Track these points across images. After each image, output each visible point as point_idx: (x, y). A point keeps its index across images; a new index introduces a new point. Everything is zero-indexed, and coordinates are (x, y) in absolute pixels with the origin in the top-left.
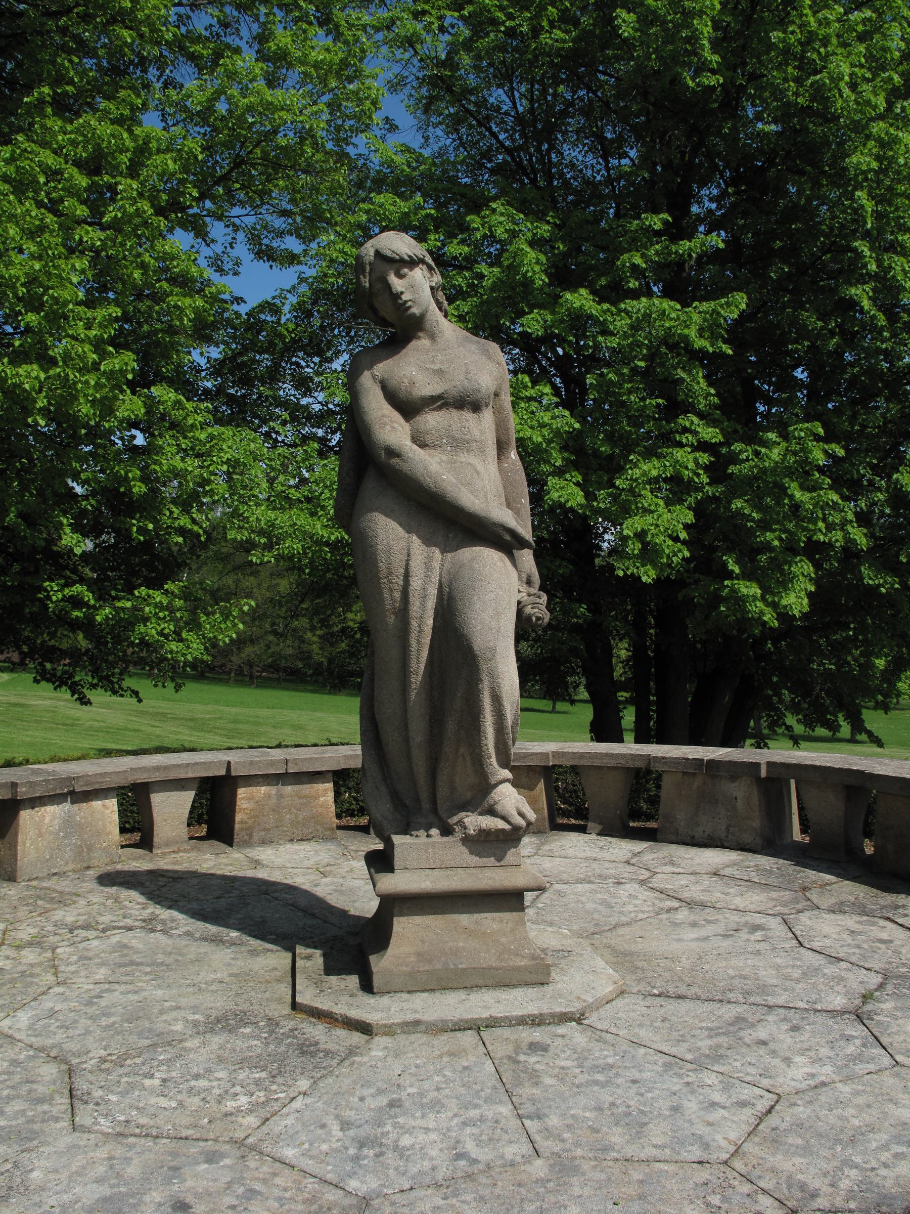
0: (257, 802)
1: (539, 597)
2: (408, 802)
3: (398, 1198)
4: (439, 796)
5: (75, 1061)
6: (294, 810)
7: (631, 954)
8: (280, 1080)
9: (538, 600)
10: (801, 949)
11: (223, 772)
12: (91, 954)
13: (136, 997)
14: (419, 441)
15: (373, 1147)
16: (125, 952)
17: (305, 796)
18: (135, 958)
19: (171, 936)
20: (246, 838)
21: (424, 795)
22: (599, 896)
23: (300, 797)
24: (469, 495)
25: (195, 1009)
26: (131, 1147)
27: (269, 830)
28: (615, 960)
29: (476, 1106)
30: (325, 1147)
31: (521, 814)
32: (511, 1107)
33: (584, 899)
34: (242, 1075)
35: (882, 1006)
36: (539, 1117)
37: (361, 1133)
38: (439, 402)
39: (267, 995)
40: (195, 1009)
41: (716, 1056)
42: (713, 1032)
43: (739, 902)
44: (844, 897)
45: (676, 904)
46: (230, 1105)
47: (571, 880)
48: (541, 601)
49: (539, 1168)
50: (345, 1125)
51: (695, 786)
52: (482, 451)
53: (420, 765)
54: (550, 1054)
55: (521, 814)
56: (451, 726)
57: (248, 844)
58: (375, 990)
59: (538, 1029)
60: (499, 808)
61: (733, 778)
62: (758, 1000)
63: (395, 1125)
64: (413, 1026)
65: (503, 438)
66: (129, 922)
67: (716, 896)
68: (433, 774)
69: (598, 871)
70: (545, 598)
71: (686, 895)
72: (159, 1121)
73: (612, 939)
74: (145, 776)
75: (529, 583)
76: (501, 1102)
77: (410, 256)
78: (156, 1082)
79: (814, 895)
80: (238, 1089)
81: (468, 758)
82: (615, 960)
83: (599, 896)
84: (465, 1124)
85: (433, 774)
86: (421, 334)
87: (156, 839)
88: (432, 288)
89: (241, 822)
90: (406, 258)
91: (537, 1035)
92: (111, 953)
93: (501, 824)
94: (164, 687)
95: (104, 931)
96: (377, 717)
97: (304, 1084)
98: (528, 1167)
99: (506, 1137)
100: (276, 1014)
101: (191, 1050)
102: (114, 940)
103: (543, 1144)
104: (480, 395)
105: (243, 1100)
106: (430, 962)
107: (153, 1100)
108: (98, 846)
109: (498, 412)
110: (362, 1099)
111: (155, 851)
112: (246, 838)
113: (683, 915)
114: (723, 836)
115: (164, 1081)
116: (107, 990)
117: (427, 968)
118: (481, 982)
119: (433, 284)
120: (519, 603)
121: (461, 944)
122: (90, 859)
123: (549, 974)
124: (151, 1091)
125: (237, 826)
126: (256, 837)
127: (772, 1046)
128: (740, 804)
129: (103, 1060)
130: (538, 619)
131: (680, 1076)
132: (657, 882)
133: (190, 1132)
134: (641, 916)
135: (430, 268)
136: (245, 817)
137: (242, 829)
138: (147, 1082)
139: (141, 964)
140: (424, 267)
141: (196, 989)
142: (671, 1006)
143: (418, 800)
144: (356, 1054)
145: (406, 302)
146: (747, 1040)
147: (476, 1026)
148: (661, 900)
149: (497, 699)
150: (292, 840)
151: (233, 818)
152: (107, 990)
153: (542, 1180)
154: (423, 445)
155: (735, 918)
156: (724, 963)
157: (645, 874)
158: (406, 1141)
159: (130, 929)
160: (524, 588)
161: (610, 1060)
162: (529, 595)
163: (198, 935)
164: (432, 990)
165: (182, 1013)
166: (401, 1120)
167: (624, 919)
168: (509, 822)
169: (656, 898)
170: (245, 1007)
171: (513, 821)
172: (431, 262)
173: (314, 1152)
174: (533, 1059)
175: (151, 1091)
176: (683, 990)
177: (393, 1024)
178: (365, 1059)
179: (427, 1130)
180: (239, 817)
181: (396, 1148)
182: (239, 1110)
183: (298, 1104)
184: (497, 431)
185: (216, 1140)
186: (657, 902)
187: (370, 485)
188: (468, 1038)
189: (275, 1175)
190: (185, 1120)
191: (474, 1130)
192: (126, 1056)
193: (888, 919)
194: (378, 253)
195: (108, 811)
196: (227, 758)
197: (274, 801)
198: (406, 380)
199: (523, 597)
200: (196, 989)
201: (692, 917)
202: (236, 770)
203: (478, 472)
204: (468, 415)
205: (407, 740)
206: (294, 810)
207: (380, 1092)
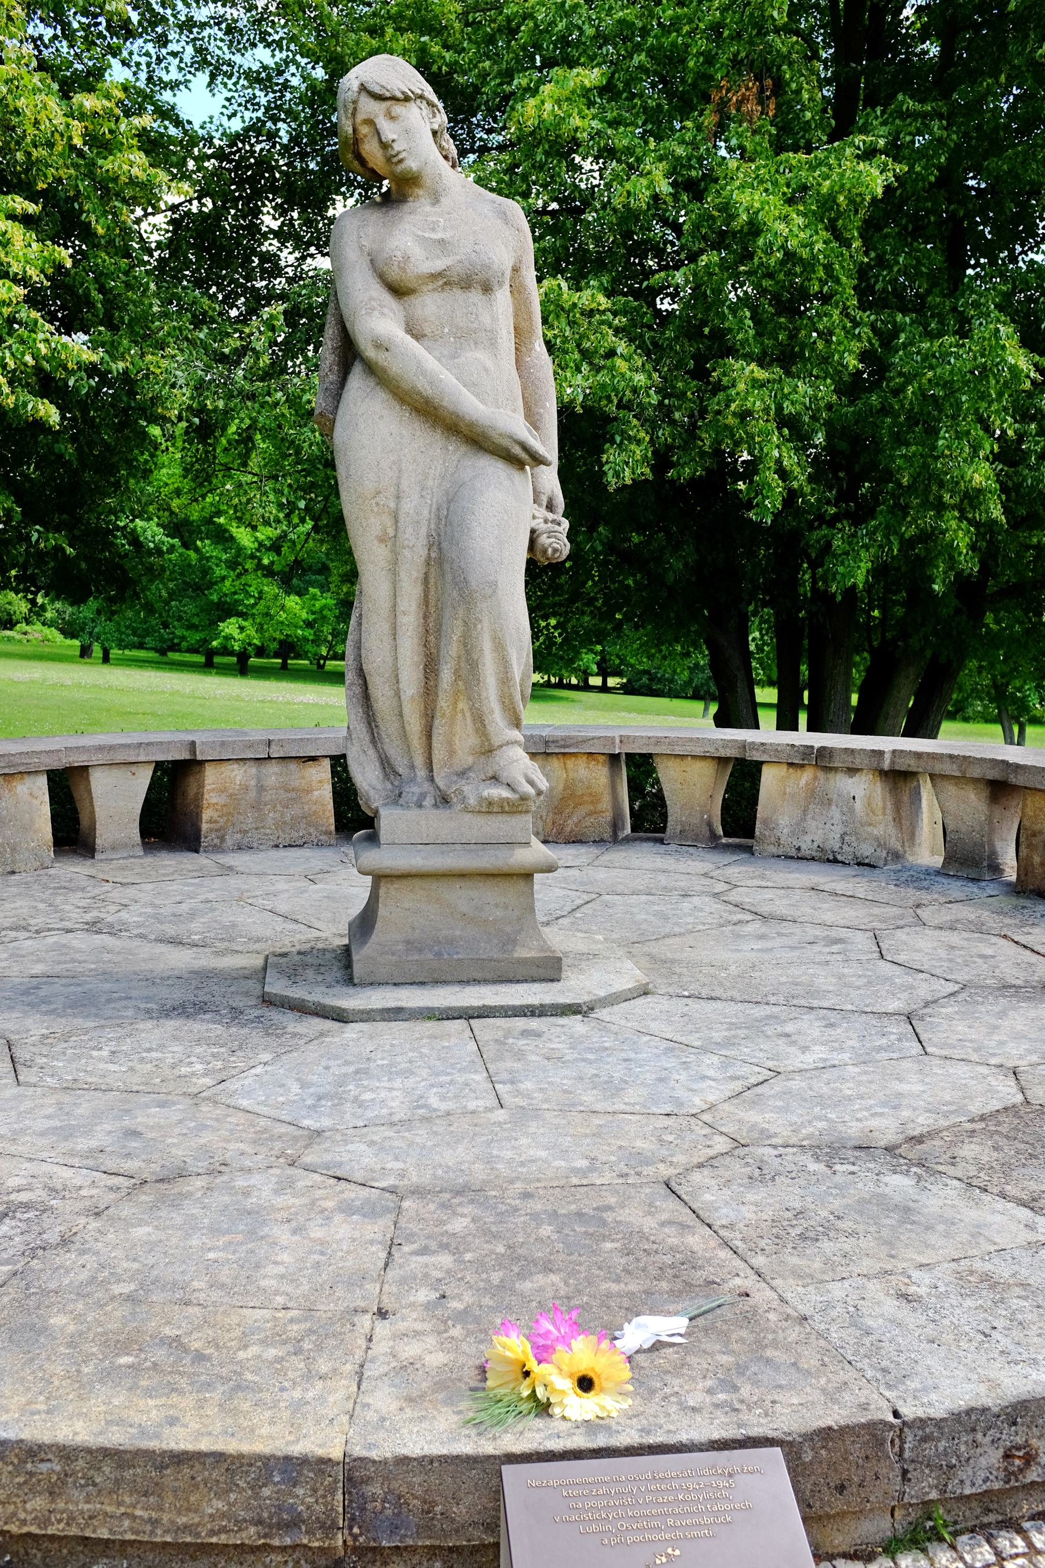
0: (231, 795)
1: (559, 524)
2: (401, 771)
3: (351, 1131)
4: (435, 761)
5: (13, 1037)
6: (279, 807)
7: (673, 961)
8: (239, 1053)
9: (557, 528)
10: (881, 963)
11: (185, 755)
12: (23, 952)
13: (79, 989)
14: (414, 331)
15: (332, 1099)
16: (64, 951)
17: (293, 790)
18: (77, 956)
19: (120, 938)
20: (217, 841)
21: (419, 760)
22: (656, 908)
23: (287, 791)
24: (473, 398)
25: (148, 999)
26: (79, 1097)
27: (246, 832)
28: (648, 966)
29: (448, 1074)
30: (281, 1099)
31: (531, 783)
32: (485, 1074)
33: (635, 910)
34: (198, 1050)
35: (943, 1010)
36: (512, 1083)
37: (321, 1090)
38: (444, 280)
39: (233, 989)
40: (148, 999)
41: (728, 1043)
42: (732, 1026)
43: (829, 917)
44: (959, 916)
45: (749, 917)
46: (184, 1070)
47: (626, 891)
48: (560, 529)
49: (500, 1115)
50: (304, 1085)
51: (803, 782)
52: (492, 343)
53: (414, 724)
54: (544, 1038)
55: (531, 783)
56: (446, 675)
57: (218, 849)
58: (356, 981)
59: (537, 1019)
60: (504, 776)
61: (852, 771)
62: (803, 1002)
63: (358, 1086)
64: (395, 1014)
65: (524, 324)
66: (68, 925)
67: (805, 911)
68: (428, 734)
69: (664, 883)
70: (566, 524)
71: (765, 909)
72: (107, 1080)
73: (654, 948)
74: (85, 758)
75: (550, 507)
76: (476, 1071)
77: (403, 93)
78: (105, 1053)
79: (924, 913)
80: (194, 1059)
81: (468, 714)
82: (648, 966)
83: (656, 908)
84: (432, 1086)
85: (428, 734)
86: (421, 192)
87: (98, 841)
88: (435, 133)
89: (210, 822)
90: (400, 95)
91: (534, 1023)
92: (47, 951)
93: (506, 793)
94: (106, 659)
95: (37, 932)
96: (364, 667)
97: (266, 1057)
98: (489, 1115)
99: (473, 1095)
100: (241, 1004)
101: (143, 1031)
102: (50, 940)
103: (507, 1099)
104: (490, 273)
105: (199, 1067)
106: (420, 951)
107: (101, 1066)
108: (24, 846)
109: (517, 290)
110: (327, 1068)
111: (98, 856)
112: (217, 841)
113: (755, 927)
114: (836, 848)
115: (113, 1052)
116: (45, 983)
117: (416, 957)
118: (478, 976)
119: (436, 127)
120: (533, 531)
121: (458, 933)
122: (14, 862)
123: (560, 969)
124: (100, 1059)
125: (205, 827)
126: (229, 841)
127: (794, 1038)
128: (858, 805)
129: (45, 1037)
130: (555, 550)
131: (678, 1057)
132: (734, 896)
133: (140, 1088)
134: (702, 927)
135: (431, 104)
136: (215, 815)
137: (211, 830)
138: (95, 1053)
139: (85, 961)
140: (424, 105)
141: (149, 983)
142: (695, 1005)
143: (412, 767)
144: (327, 1036)
145: (399, 153)
146: (769, 1033)
147: (469, 1014)
148: (730, 913)
149: (499, 647)
150: (277, 846)
151: (198, 816)
152: (45, 983)
153: (500, 1123)
154: (418, 337)
155: (818, 932)
156: (780, 972)
157: (720, 887)
158: (367, 1096)
159: (69, 931)
160: (542, 512)
161: (607, 1045)
162: (546, 521)
163: (153, 937)
164: (423, 983)
165: (134, 1002)
166: (365, 1083)
167: (677, 930)
168: (513, 790)
169: (725, 911)
170: (206, 999)
171: (520, 789)
172: (434, 98)
173: (270, 1102)
174: (521, 1042)
175: (100, 1059)
176: (718, 992)
177: (372, 1010)
178: (336, 1039)
179: (391, 1089)
180: (206, 815)
181: (356, 1100)
182: (193, 1074)
183: (259, 1070)
184: (516, 316)
185: (169, 1093)
186: (725, 915)
187: (357, 380)
188: (460, 1024)
189: (228, 1116)
190: (136, 1079)
191: (440, 1090)
192: (70, 1035)
193: (1005, 937)
194: (363, 88)
195: (36, 802)
196: (191, 738)
197: (252, 794)
198: (398, 254)
199: (542, 526)
200: (149, 983)
201: (764, 930)
202: (202, 754)
203: (486, 370)
204: (475, 296)
205: (398, 694)
206: (279, 807)
207: (347, 1063)
